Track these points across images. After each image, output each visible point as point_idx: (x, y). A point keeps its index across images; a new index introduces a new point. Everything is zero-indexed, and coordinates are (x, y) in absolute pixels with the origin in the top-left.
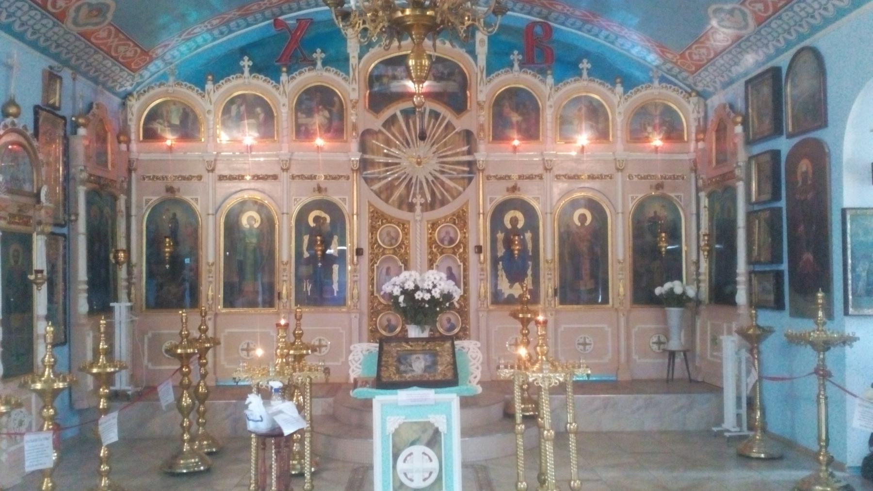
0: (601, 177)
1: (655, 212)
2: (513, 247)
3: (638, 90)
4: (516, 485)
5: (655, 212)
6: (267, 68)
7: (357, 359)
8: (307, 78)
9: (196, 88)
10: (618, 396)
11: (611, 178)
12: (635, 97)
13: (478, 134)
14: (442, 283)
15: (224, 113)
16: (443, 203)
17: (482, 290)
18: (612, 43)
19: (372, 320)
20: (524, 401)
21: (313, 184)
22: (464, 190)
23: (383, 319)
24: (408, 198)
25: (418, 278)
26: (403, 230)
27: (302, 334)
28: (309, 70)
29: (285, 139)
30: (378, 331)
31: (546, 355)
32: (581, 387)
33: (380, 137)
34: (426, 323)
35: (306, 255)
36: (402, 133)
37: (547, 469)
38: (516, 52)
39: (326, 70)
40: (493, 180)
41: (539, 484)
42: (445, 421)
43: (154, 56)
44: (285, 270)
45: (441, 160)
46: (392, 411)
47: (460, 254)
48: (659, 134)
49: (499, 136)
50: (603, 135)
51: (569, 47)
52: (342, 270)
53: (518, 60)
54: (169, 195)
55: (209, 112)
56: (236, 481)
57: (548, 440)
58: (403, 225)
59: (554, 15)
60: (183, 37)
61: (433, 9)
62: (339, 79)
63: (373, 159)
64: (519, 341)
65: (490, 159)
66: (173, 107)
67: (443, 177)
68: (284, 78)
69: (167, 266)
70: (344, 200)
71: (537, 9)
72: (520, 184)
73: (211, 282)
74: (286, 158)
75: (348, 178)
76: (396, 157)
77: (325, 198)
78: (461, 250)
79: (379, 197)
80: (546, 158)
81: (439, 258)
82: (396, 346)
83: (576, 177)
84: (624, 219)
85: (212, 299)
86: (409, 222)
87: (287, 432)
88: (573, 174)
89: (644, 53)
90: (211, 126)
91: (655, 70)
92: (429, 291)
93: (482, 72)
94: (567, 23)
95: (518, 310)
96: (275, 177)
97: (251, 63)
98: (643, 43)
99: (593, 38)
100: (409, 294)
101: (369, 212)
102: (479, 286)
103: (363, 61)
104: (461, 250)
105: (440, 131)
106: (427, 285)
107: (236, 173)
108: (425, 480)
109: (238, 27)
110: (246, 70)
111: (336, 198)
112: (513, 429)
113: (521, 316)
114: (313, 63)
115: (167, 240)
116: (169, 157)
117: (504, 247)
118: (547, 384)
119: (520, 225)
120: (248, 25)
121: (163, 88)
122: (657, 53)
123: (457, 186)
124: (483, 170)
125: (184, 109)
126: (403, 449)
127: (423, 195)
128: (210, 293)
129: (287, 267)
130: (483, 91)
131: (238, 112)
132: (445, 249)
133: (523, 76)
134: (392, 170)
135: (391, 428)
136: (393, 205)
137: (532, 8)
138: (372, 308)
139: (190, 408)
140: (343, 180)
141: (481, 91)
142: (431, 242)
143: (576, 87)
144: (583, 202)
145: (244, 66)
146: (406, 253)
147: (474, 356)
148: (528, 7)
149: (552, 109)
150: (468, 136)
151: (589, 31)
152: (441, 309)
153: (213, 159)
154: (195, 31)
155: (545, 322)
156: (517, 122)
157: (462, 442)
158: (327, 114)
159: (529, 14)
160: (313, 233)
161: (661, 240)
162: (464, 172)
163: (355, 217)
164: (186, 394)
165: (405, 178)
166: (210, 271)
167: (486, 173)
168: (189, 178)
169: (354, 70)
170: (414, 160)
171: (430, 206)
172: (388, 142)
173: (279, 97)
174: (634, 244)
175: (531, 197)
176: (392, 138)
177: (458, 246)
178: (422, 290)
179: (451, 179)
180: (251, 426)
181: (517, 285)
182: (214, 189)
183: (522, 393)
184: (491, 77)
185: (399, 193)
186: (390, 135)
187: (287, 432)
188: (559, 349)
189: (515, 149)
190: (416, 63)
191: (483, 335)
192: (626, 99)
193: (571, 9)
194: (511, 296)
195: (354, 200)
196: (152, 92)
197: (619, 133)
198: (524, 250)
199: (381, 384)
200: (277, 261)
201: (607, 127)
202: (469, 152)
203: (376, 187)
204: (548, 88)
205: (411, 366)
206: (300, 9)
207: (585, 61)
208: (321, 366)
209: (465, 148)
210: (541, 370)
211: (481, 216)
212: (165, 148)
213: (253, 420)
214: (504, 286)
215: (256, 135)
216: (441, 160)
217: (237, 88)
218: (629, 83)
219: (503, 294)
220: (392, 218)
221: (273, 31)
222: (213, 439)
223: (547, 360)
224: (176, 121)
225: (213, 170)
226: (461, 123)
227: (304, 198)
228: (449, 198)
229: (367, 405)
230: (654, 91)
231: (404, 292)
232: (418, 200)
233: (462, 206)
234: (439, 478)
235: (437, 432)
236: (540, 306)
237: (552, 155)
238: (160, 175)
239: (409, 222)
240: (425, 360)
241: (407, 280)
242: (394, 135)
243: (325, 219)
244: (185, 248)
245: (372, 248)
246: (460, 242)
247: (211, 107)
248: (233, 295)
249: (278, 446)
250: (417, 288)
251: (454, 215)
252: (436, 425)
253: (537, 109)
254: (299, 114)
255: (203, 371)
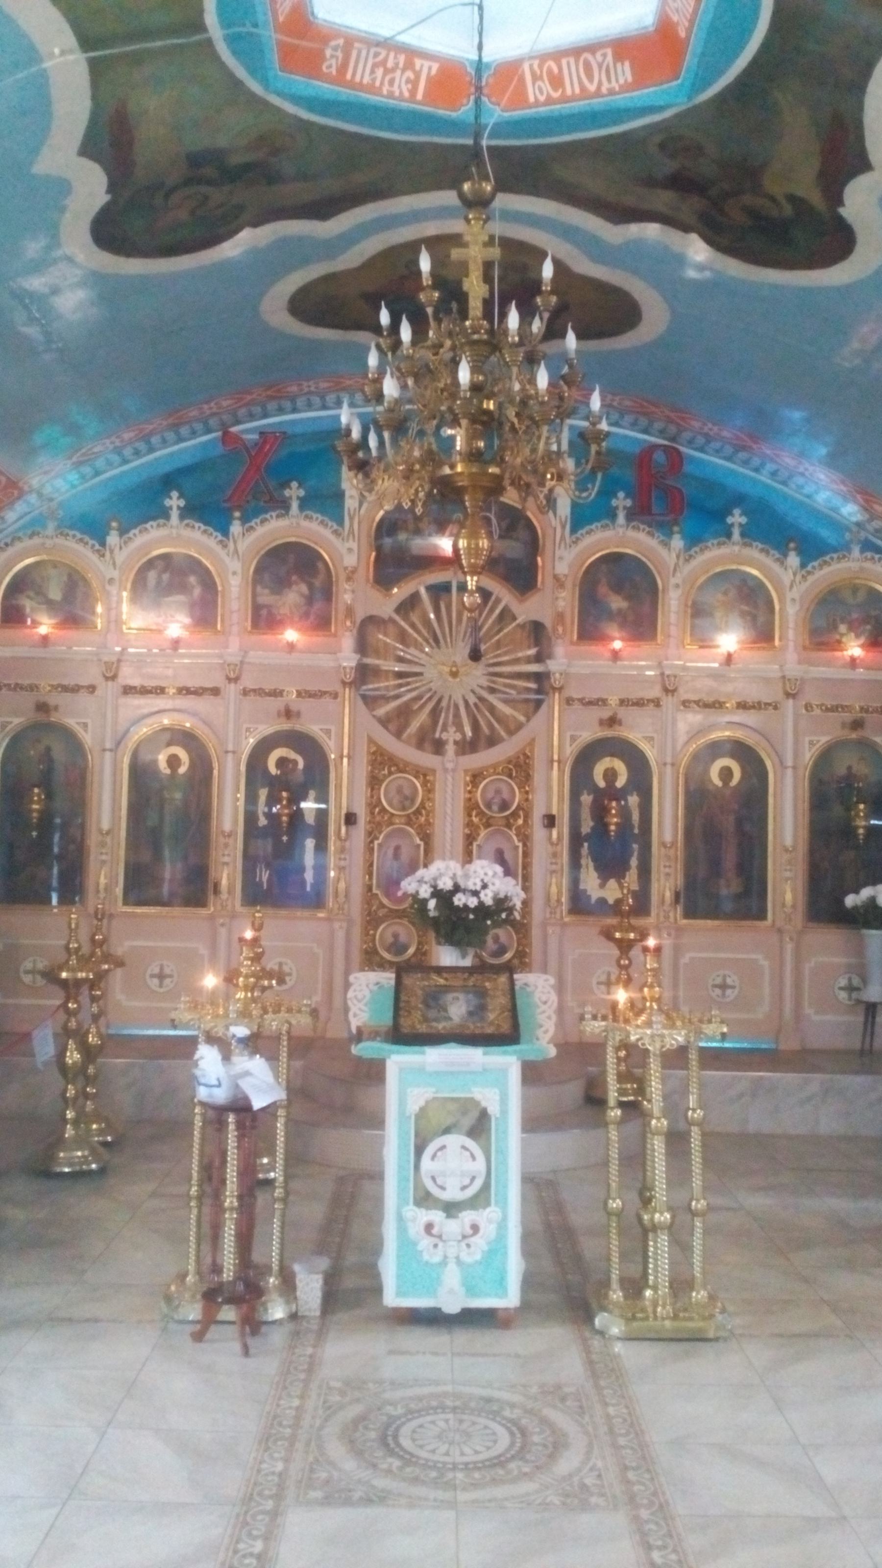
0: (758, 706)
1: (849, 768)
2: (607, 820)
3: (825, 562)
4: (606, 1204)
5: (849, 768)
6: (212, 509)
7: (360, 996)
8: (274, 529)
9: (91, 542)
10: (778, 1075)
11: (776, 708)
12: (819, 574)
13: (555, 629)
14: (497, 882)
15: (135, 584)
16: (493, 741)
17: (554, 889)
18: (784, 483)
19: (367, 934)
20: (622, 1078)
21: (277, 704)
22: (528, 720)
23: (385, 932)
24: (434, 731)
25: (459, 872)
26: (424, 784)
27: (263, 953)
28: (278, 516)
29: (235, 629)
30: (376, 952)
31: (658, 1000)
32: (713, 1058)
33: (391, 629)
34: (469, 944)
35: (263, 821)
36: (427, 622)
37: (655, 1180)
38: (621, 495)
39: (306, 517)
40: (577, 706)
41: (641, 1205)
42: (497, 1098)
43: (26, 488)
44: (226, 845)
45: (491, 669)
46: (414, 1078)
47: (518, 829)
48: (857, 636)
49: (589, 632)
50: (763, 635)
51: (710, 486)
52: (321, 847)
53: (625, 508)
54: (41, 717)
55: (111, 581)
56: (151, 1187)
57: (658, 1134)
58: (425, 775)
59: (687, 435)
60: (74, 459)
61: (498, 465)
62: (327, 533)
63: (378, 666)
64: (613, 978)
65: (573, 670)
66: (52, 572)
67: (492, 698)
68: (236, 528)
69: (34, 834)
70: (328, 732)
71: (658, 425)
72: (622, 713)
73: (104, 862)
74: (236, 660)
75: (335, 696)
76: (416, 663)
77: (298, 727)
78: (520, 822)
79: (387, 728)
80: (667, 672)
81: (483, 833)
82: (423, 979)
83: (716, 705)
84: (795, 777)
85: (106, 890)
86: (434, 771)
87: (258, 1103)
88: (711, 699)
89: (837, 501)
90: (114, 605)
91: (855, 529)
92: (475, 893)
93: (563, 527)
94: (706, 448)
95: (613, 926)
96: (215, 692)
97: (182, 503)
98: (835, 486)
99: (753, 474)
100: (444, 897)
101: (369, 753)
102: (550, 878)
103: (364, 502)
104: (520, 822)
105: (490, 621)
106: (473, 883)
107: (150, 683)
108: (464, 1188)
109: (165, 443)
110: (175, 514)
111: (315, 729)
112: (604, 1124)
113: (618, 935)
114: (284, 506)
115: (36, 790)
116: (39, 652)
117: (593, 819)
118: (658, 1045)
119: (620, 783)
120: (181, 440)
121: (36, 540)
122: (855, 502)
123: (516, 714)
124: (560, 689)
125: (70, 576)
126: (431, 1140)
127: (460, 727)
128: (103, 881)
129: (231, 841)
130: (566, 557)
131: (159, 582)
132: (495, 821)
133: (631, 533)
134: (408, 684)
135: (413, 1106)
136: (407, 742)
137: (651, 423)
138: (369, 914)
139: (81, 1070)
140: (327, 699)
141: (561, 558)
142: (471, 807)
143: (717, 555)
144: (728, 746)
145: (171, 508)
146: (429, 824)
147: (544, 998)
148: (643, 422)
149: (679, 592)
150: (537, 632)
151: (745, 463)
152: (493, 922)
153: (114, 659)
154: (95, 450)
155: (658, 950)
156: (620, 611)
157: (523, 1139)
158: (304, 588)
159: (645, 431)
160: (276, 785)
161: (857, 815)
162: (528, 690)
163: (345, 760)
164: (71, 1044)
165: (430, 698)
166: (103, 844)
167: (567, 693)
168: (75, 689)
169: (351, 519)
170: (446, 669)
171: (468, 747)
172: (403, 637)
173: (227, 560)
174: (812, 823)
175: (639, 736)
176: (410, 631)
177: (515, 815)
178: (464, 891)
179: (506, 701)
180: (202, 1093)
181: (612, 883)
182: (116, 709)
183: (618, 1064)
184: (578, 535)
185: (419, 722)
186: (407, 627)
187: (258, 1103)
188: (681, 994)
189: (616, 655)
190: (469, 544)
191: (553, 963)
192: (804, 577)
193: (716, 428)
194: (602, 901)
195: (344, 732)
196: (19, 546)
197: (791, 634)
198: (625, 824)
199: (401, 1036)
200: (214, 829)
201: (771, 623)
202: (539, 658)
203: (381, 711)
204: (674, 555)
205: (446, 1010)
206: (265, 416)
207: (737, 512)
208: (306, 1005)
209: (532, 652)
210: (649, 1024)
211: (556, 765)
212: (36, 637)
213: (206, 1085)
214: (590, 881)
215: (187, 620)
216: (491, 669)
217: (159, 542)
218: (812, 549)
219: (589, 897)
220: (407, 764)
221: (220, 450)
222: (107, 1120)
223: (660, 1009)
224: (55, 593)
225: (114, 678)
226: (527, 610)
227: (261, 727)
228: (503, 733)
229: (375, 1072)
230: (849, 566)
231: (437, 893)
232: (451, 736)
233: (524, 749)
234: (486, 1186)
235: (484, 1115)
236: (651, 920)
237: (677, 666)
238: (26, 682)
239: (434, 771)
240: (468, 1002)
241: (441, 875)
242: (413, 626)
243: (295, 762)
244: (59, 804)
245: (372, 813)
246: (519, 807)
247: (115, 574)
248: (140, 885)
249: (240, 1126)
250: (457, 889)
251: (509, 762)
252: (484, 1104)
253: (653, 591)
254: (259, 589)
255: (95, 1009)
